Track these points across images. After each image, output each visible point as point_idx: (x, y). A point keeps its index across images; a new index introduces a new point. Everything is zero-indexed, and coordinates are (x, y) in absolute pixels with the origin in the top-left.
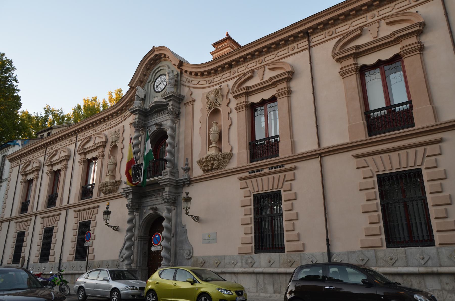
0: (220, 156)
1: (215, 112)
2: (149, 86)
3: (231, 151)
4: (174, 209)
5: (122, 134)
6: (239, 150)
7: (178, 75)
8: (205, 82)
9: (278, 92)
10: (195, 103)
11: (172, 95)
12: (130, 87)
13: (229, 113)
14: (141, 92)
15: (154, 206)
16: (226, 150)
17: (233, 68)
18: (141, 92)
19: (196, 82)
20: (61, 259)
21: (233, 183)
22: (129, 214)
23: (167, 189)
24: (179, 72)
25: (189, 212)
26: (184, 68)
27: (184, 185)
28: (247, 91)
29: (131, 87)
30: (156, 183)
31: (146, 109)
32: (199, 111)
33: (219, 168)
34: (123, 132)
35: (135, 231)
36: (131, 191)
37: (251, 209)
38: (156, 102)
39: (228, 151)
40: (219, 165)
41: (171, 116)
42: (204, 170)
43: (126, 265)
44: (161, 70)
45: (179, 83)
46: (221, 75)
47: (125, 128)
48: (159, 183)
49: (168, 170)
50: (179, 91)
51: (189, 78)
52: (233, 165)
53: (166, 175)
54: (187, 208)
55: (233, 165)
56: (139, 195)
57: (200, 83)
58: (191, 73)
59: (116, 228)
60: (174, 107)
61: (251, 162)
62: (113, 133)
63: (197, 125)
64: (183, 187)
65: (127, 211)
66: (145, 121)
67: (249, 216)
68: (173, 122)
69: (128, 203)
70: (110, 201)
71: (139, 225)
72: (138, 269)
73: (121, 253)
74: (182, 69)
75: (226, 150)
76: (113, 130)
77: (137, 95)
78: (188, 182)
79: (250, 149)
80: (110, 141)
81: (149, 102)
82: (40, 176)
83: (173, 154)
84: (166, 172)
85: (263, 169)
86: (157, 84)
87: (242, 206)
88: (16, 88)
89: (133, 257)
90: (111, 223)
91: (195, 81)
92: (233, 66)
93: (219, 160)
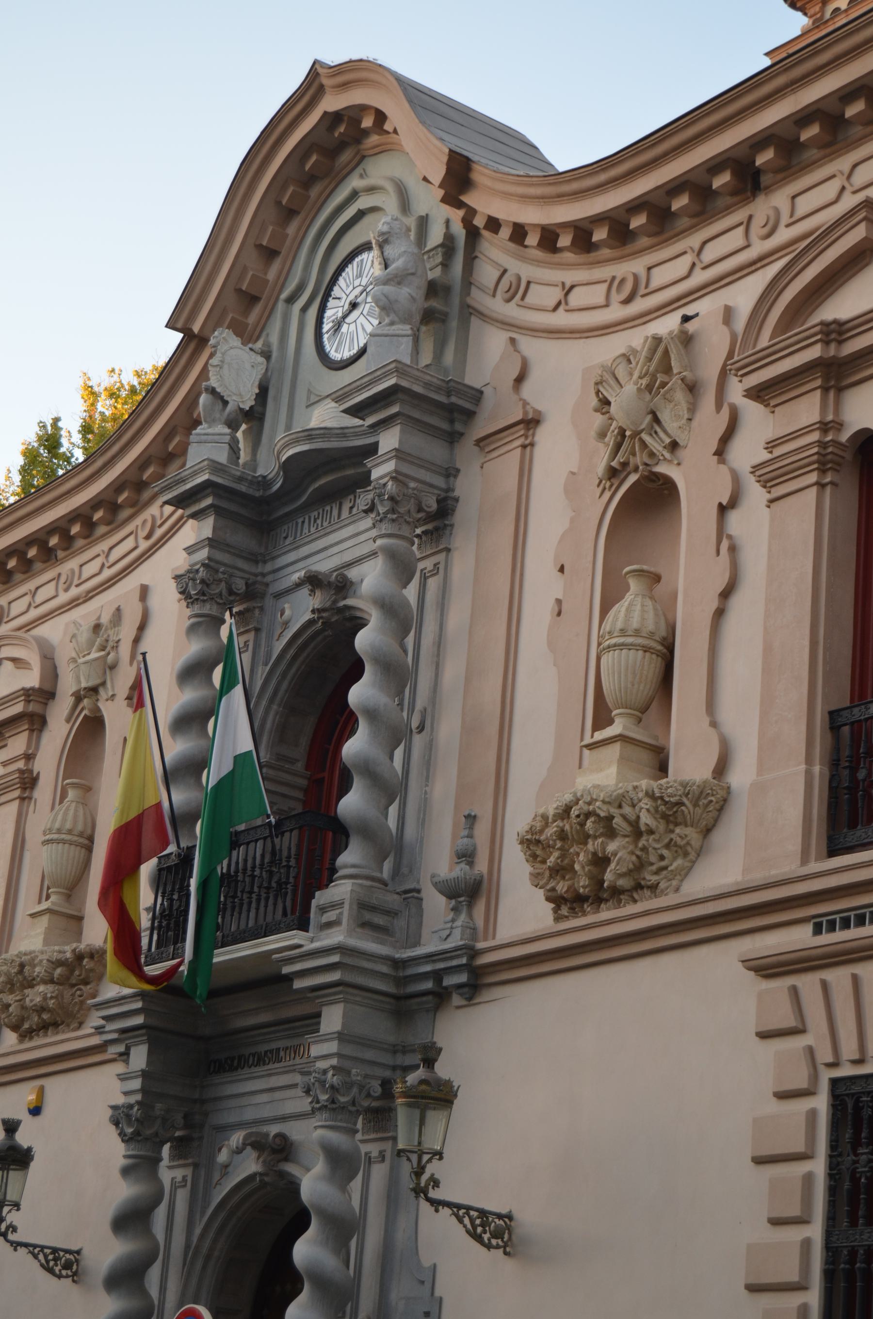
0: (646, 804)
1: (645, 500)
2: (288, 326)
3: (721, 768)
4: (382, 1157)
5: (137, 641)
6: (761, 769)
7: (448, 246)
8: (597, 295)
9: (778, 452)
10: (543, 436)
11: (207, 484)
12: (179, 336)
13: (723, 509)
14: (235, 370)
15: (274, 1130)
16: (690, 765)
17: (768, 189)
18: (235, 370)
19: (554, 295)
21: (714, 986)
22: (126, 1172)
23: (333, 1019)
24: (459, 230)
25: (435, 1182)
26: (485, 203)
27: (440, 997)
28: (832, 351)
29: (189, 336)
30: (269, 981)
31: (264, 482)
32: (557, 486)
33: (639, 887)
34: (142, 627)
35: (163, 1289)
36: (139, 1020)
37: (808, 1178)
38: (310, 435)
40: (641, 865)
41: (385, 528)
42: (556, 900)
44: (361, 214)
45: (456, 300)
46: (694, 240)
47: (154, 602)
48: (289, 979)
49: (341, 890)
50: (449, 358)
51: (515, 267)
52: (724, 869)
53: (329, 925)
55: (724, 869)
56: (198, 1045)
57: (575, 299)
58: (519, 233)
59: (62, 1263)
60: (406, 469)
61: (832, 852)
62: (84, 635)
63: (542, 586)
64: (437, 1008)
65: (115, 1150)
66: (255, 559)
67: (794, 1235)
68: (402, 568)
69: (121, 1100)
70: (50, 1084)
71: (187, 1247)
74: (471, 212)
76: (85, 614)
77: (213, 391)
78: (463, 978)
79: (834, 763)
80: (67, 686)
81: (288, 427)
83: (390, 790)
84: (333, 906)
86: (333, 312)
87: (759, 1161)
91: (546, 279)
92: (765, 180)
93: (637, 832)
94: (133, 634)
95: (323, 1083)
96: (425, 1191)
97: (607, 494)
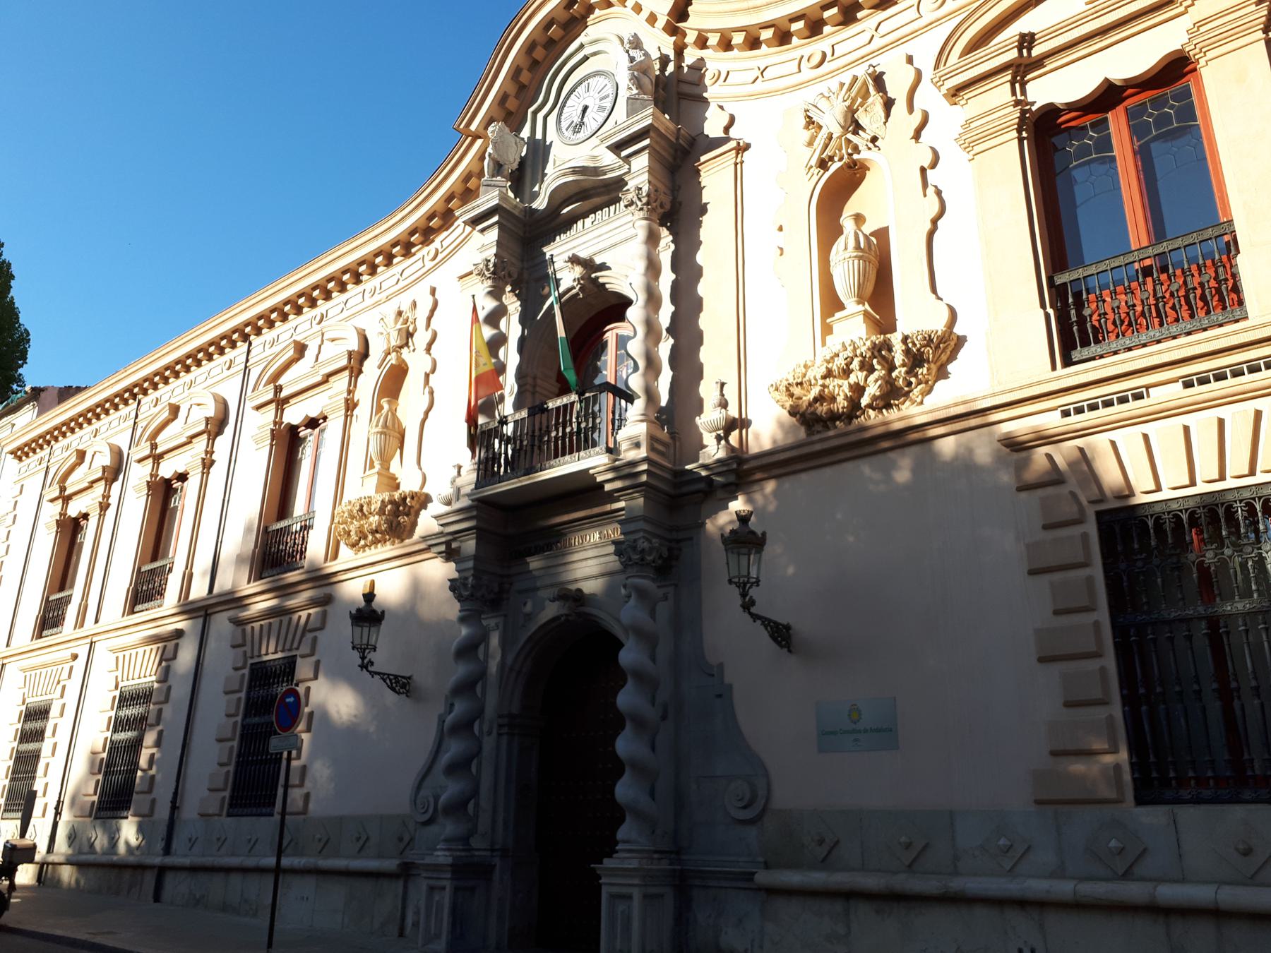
4: (497, 625)
20: (174, 807)
25: (372, 663)
39: (937, 324)
43: (446, 840)
54: (744, 586)
61: (40, 636)
72: (497, 861)
73: (419, 787)
75: (916, 315)
82: (113, 501)
85: (1148, 387)
88: (671, 68)
89: (477, 805)
90: (380, 659)
94: (427, 314)
95: (634, 548)
96: (366, 668)
97: (815, 178)
